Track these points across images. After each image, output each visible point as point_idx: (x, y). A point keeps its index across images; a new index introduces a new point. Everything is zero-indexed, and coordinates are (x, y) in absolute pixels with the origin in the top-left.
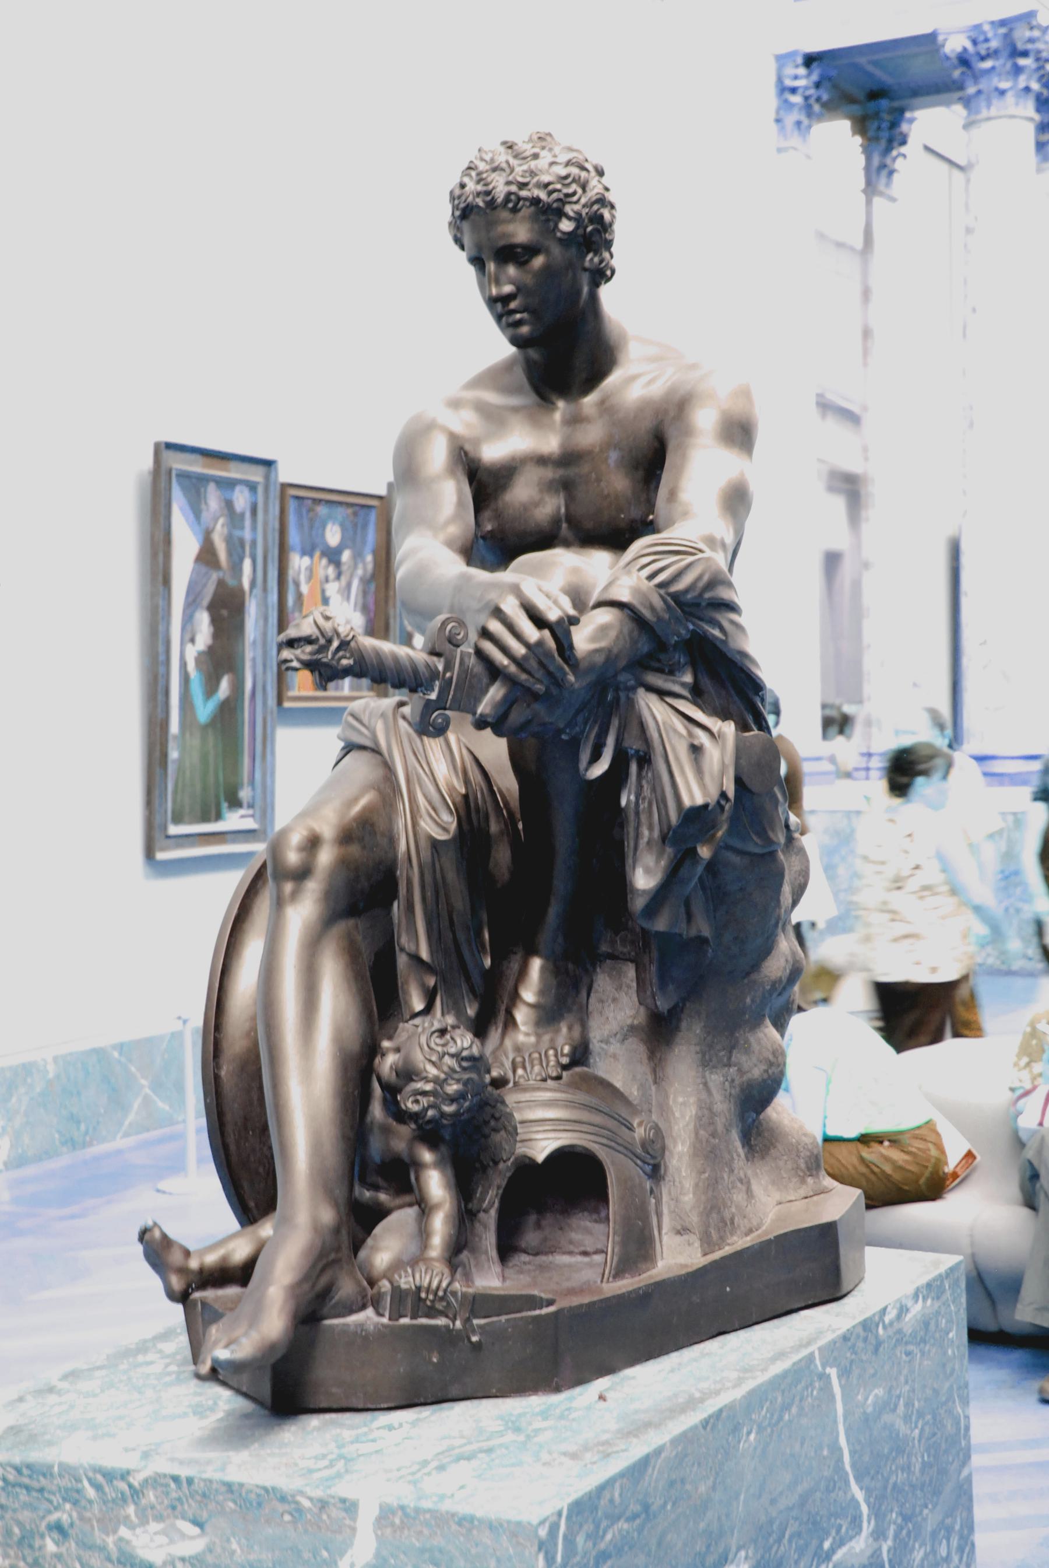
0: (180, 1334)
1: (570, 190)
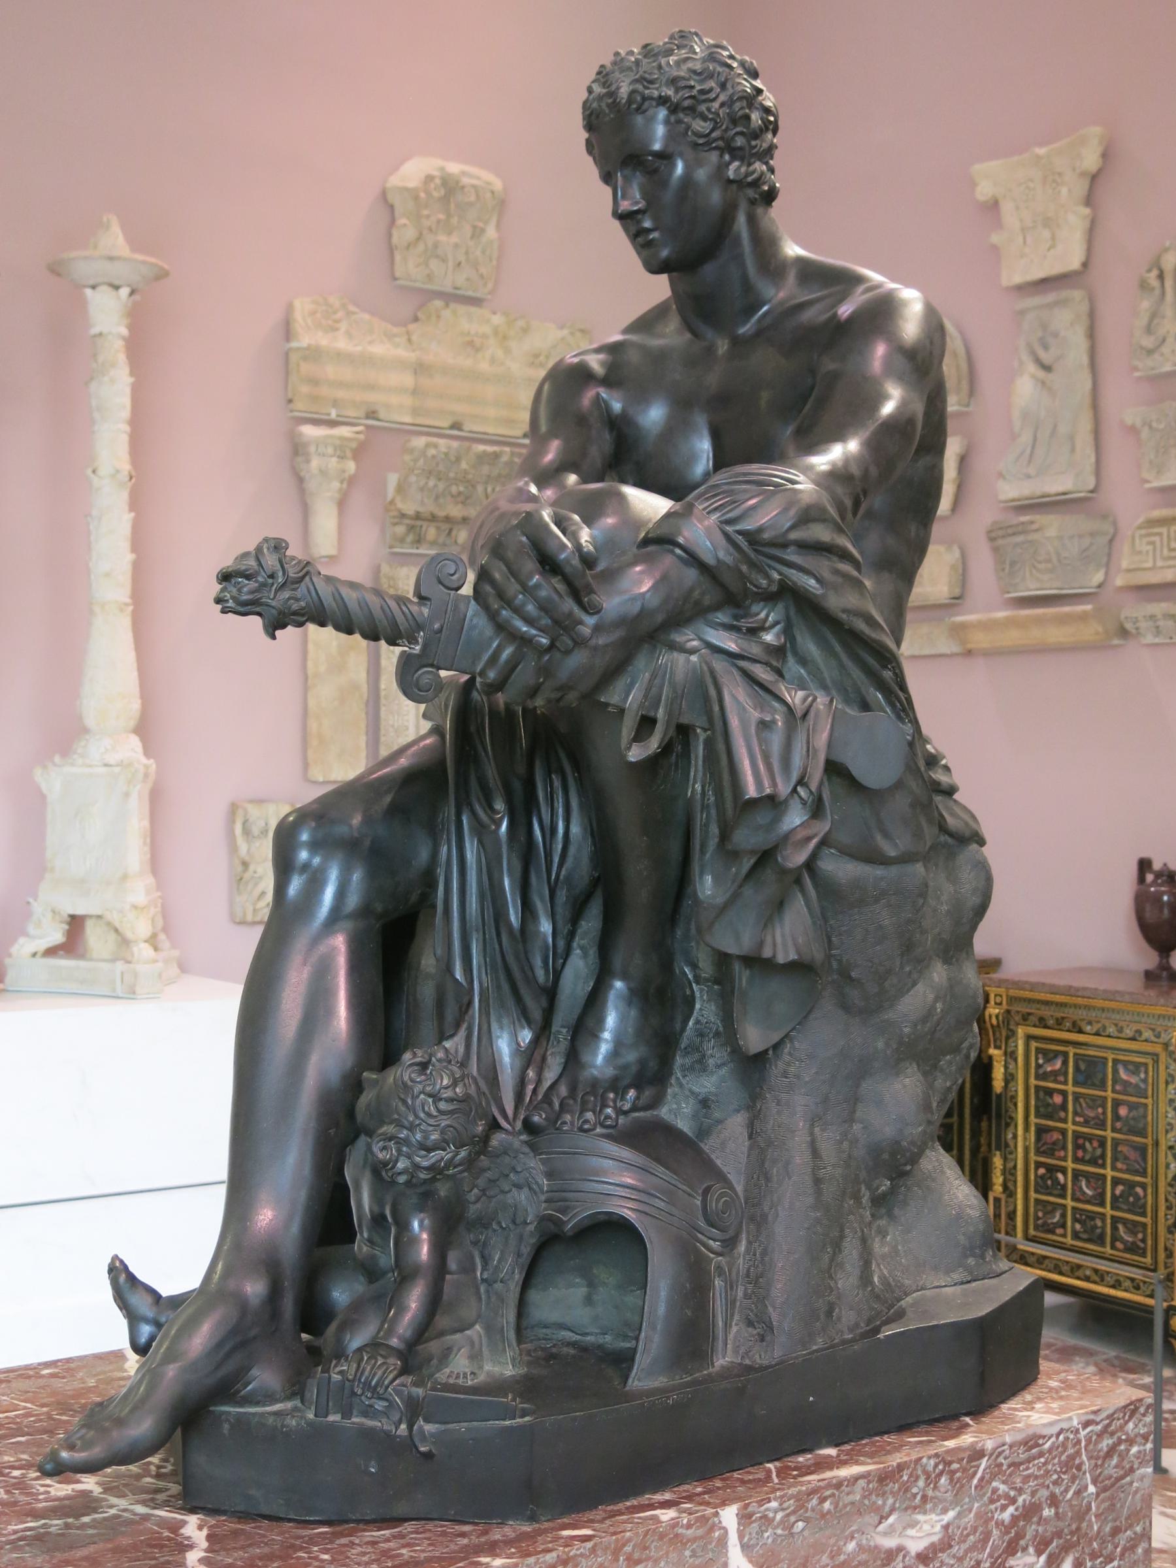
0: (1049, 1346)
1: (706, 86)
